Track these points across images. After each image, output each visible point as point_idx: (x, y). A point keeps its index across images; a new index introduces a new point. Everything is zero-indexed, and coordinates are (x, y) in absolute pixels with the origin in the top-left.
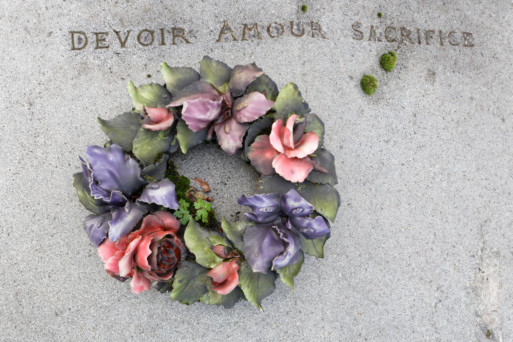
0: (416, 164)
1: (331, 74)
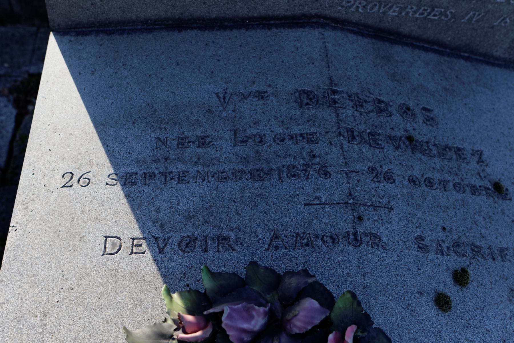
1: (397, 288)
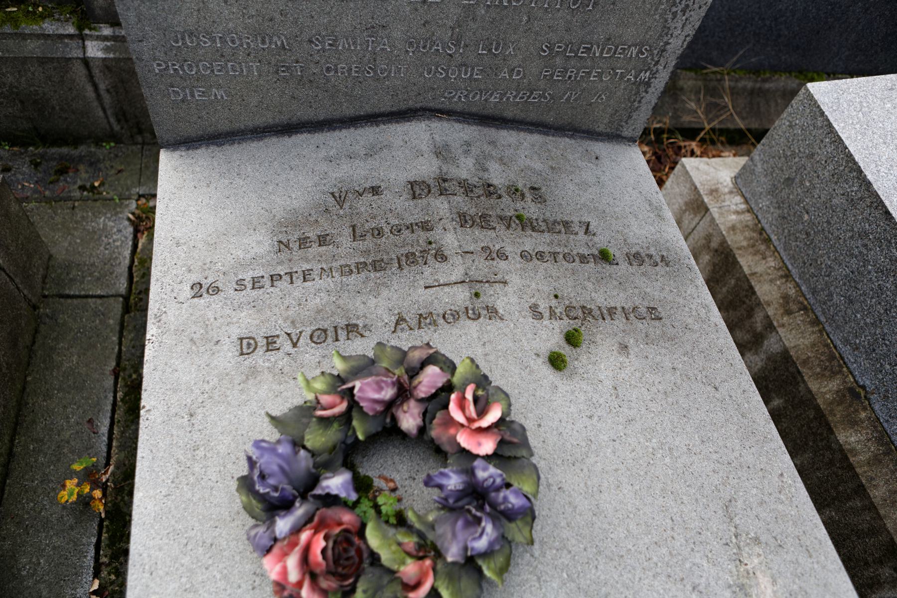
0: (629, 439)
